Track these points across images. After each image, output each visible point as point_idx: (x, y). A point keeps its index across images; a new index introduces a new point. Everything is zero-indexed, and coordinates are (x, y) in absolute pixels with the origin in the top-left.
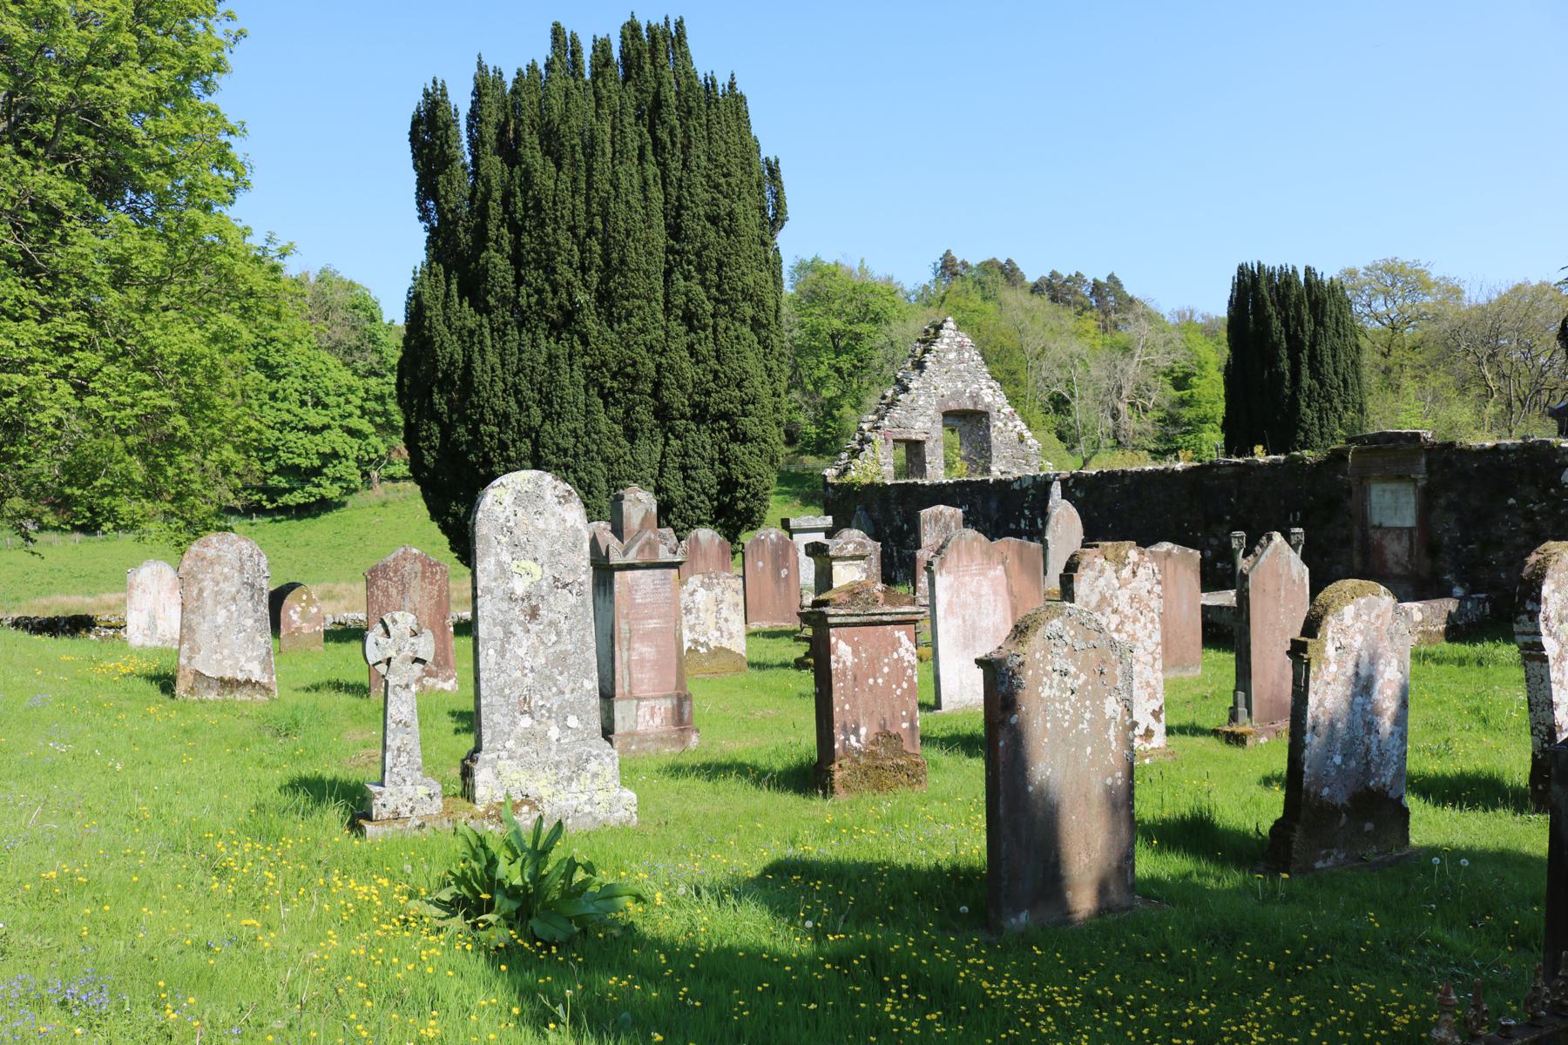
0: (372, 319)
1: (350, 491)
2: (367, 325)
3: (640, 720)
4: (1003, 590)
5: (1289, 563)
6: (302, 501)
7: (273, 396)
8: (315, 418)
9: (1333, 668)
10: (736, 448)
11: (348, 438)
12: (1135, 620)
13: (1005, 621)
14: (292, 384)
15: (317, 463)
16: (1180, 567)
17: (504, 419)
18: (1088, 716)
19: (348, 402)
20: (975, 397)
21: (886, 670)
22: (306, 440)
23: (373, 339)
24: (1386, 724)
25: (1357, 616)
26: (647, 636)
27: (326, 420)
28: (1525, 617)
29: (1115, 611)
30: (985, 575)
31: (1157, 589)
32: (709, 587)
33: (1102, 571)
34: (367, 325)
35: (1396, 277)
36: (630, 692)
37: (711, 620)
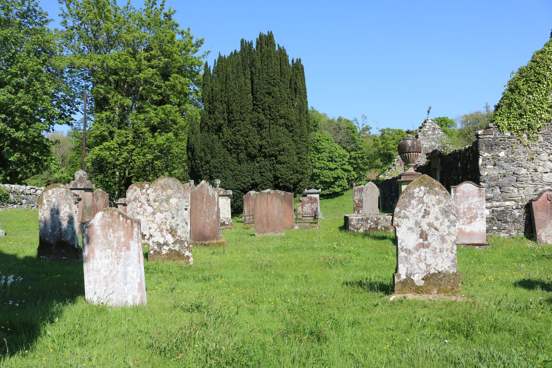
0: (354, 132)
1: (345, 190)
2: (352, 134)
5: (208, 190)
6: (328, 193)
7: (319, 159)
8: (332, 165)
9: (46, 206)
10: (278, 166)
11: (344, 172)
14: (325, 155)
15: (333, 180)
16: (274, 198)
17: (201, 159)
19: (343, 160)
22: (329, 173)
23: (353, 139)
24: (65, 224)
25: (53, 193)
27: (336, 166)
29: (139, 202)
33: (136, 190)
34: (352, 134)
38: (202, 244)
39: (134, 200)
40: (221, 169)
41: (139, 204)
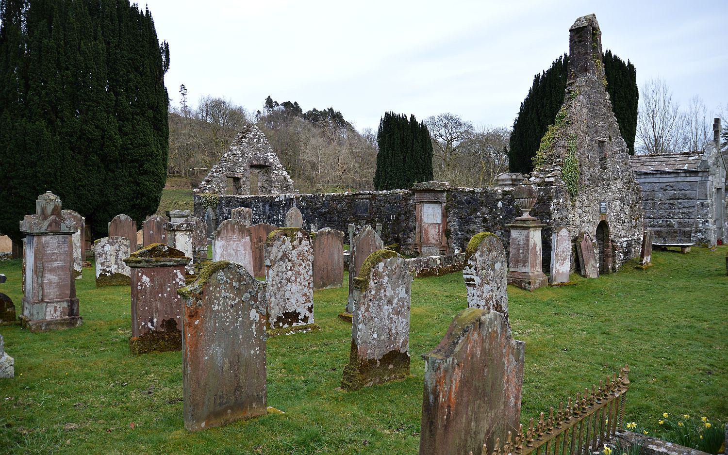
3: (48, 314)
4: (248, 248)
12: (300, 265)
13: (250, 263)
18: (240, 319)
20: (265, 160)
21: (169, 289)
25: (386, 266)
26: (53, 270)
28: (467, 267)
30: (240, 241)
31: (312, 250)
32: (112, 244)
33: (284, 242)
35: (449, 121)
36: (42, 299)
37: (113, 260)
38: (446, 427)
39: (282, 259)
40: (593, 135)
41: (290, 264)
